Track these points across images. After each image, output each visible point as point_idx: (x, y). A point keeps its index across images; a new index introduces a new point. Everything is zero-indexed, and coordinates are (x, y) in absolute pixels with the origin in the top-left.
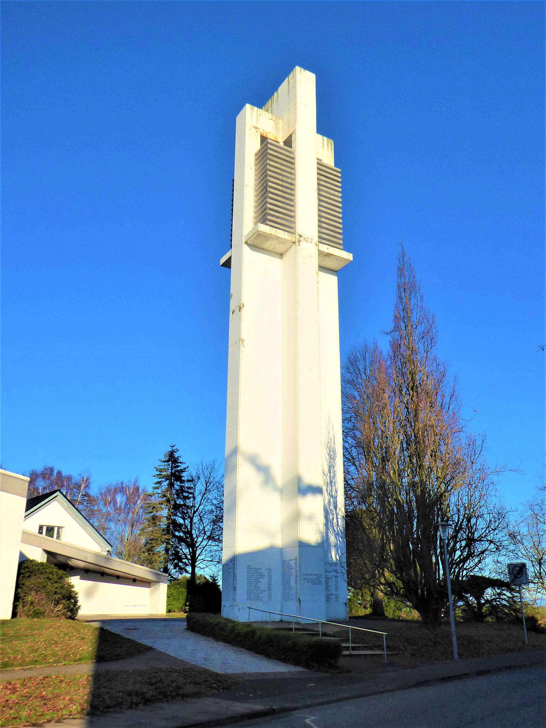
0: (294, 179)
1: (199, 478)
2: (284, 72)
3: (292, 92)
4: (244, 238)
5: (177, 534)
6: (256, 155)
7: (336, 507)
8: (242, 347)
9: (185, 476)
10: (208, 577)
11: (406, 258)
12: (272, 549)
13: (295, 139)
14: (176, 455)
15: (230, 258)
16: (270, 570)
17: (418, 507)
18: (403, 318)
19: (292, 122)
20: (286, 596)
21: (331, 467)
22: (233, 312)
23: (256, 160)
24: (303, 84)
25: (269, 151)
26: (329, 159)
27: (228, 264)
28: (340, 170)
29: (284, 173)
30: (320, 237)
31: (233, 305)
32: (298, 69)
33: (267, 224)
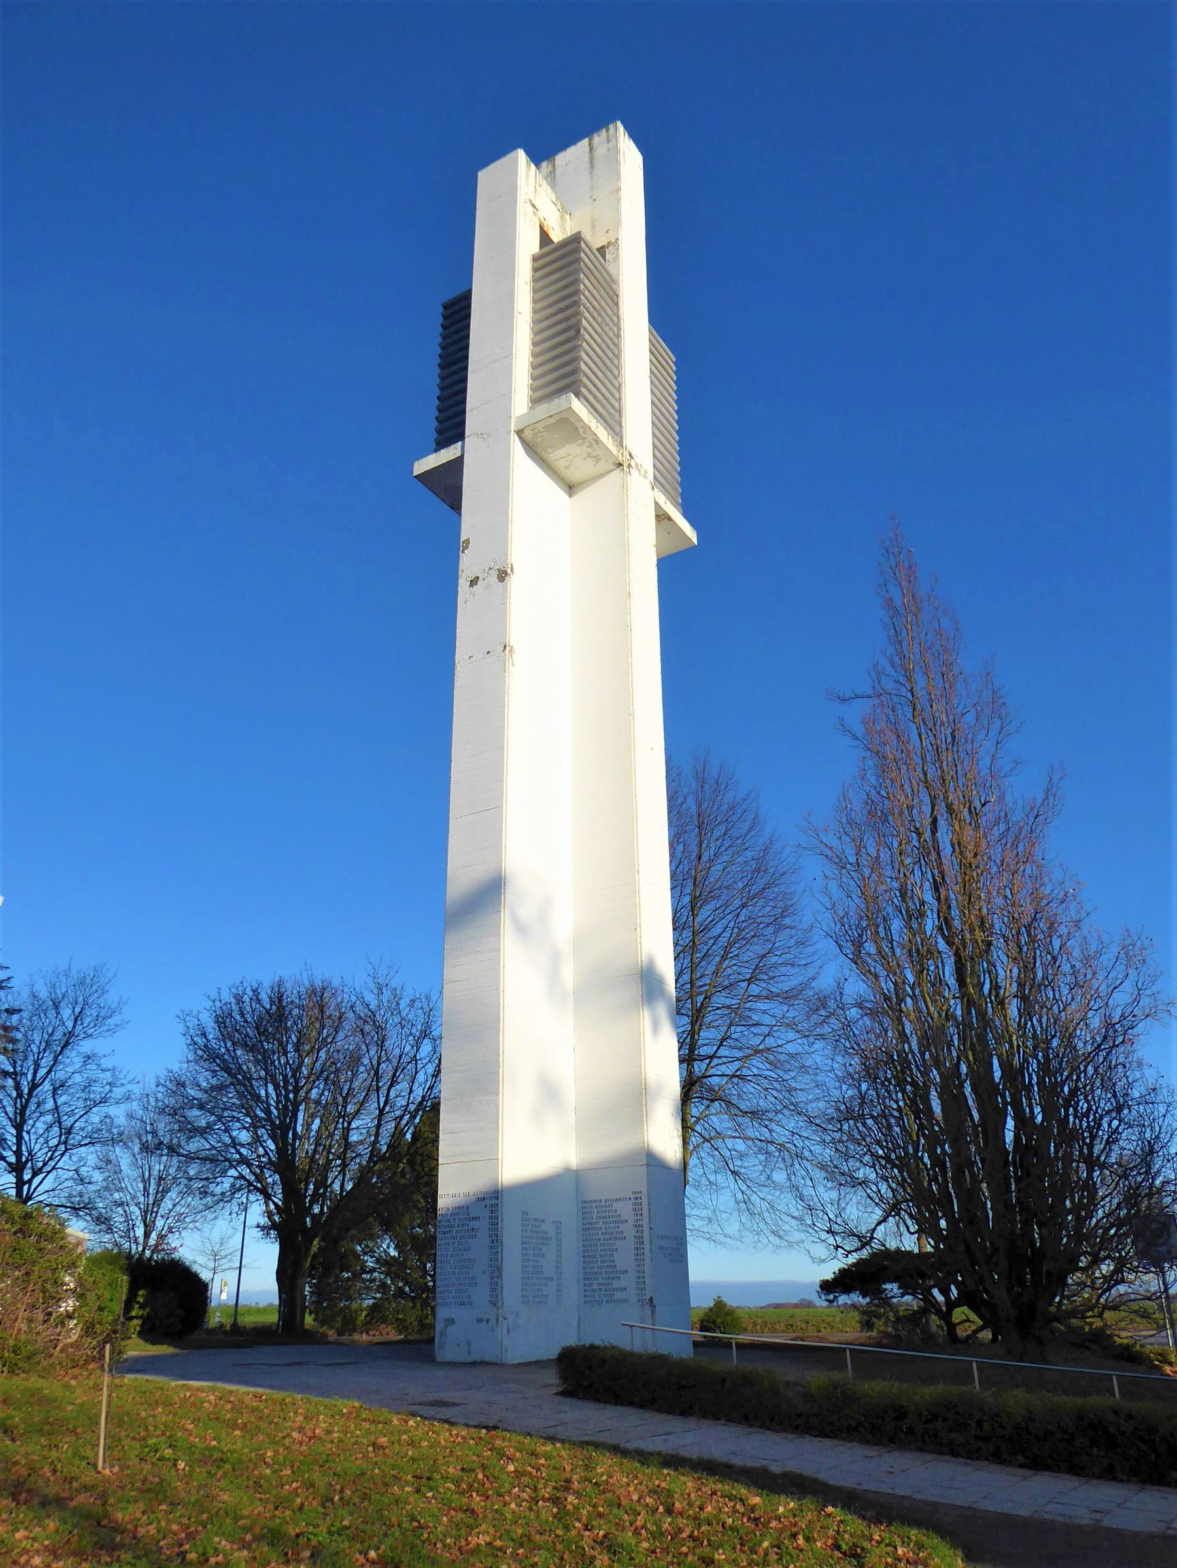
4: (513, 420)
8: (509, 667)
12: (567, 1170)
16: (558, 1224)
17: (1037, 1084)
31: (469, 564)
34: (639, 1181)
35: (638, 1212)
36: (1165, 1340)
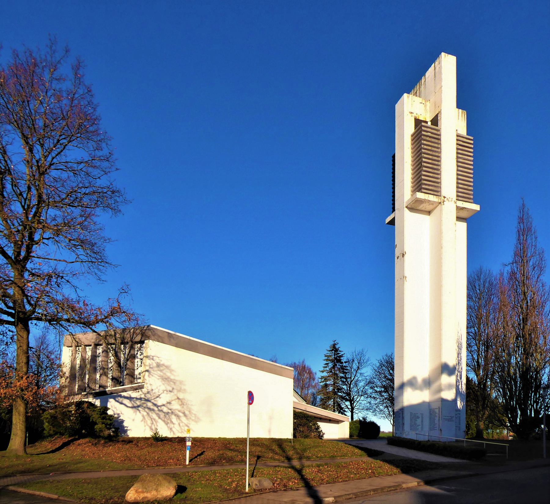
0: (440, 152)
1: (353, 360)
2: (431, 58)
3: (437, 76)
5: (340, 394)
6: (412, 136)
7: (461, 378)
8: (405, 282)
9: (344, 359)
10: (361, 419)
11: (526, 209)
12: (424, 403)
13: (441, 119)
14: (337, 347)
15: (394, 219)
16: (422, 414)
18: (521, 255)
19: (437, 105)
20: (432, 428)
21: (459, 354)
22: (398, 258)
23: (412, 140)
24: (446, 68)
25: (423, 133)
26: (463, 131)
27: (392, 222)
28: (472, 138)
29: (433, 149)
30: (458, 196)
31: (397, 252)
32: (443, 54)
33: (422, 192)
34: (439, 404)
35: (439, 411)
36: (254, 449)
